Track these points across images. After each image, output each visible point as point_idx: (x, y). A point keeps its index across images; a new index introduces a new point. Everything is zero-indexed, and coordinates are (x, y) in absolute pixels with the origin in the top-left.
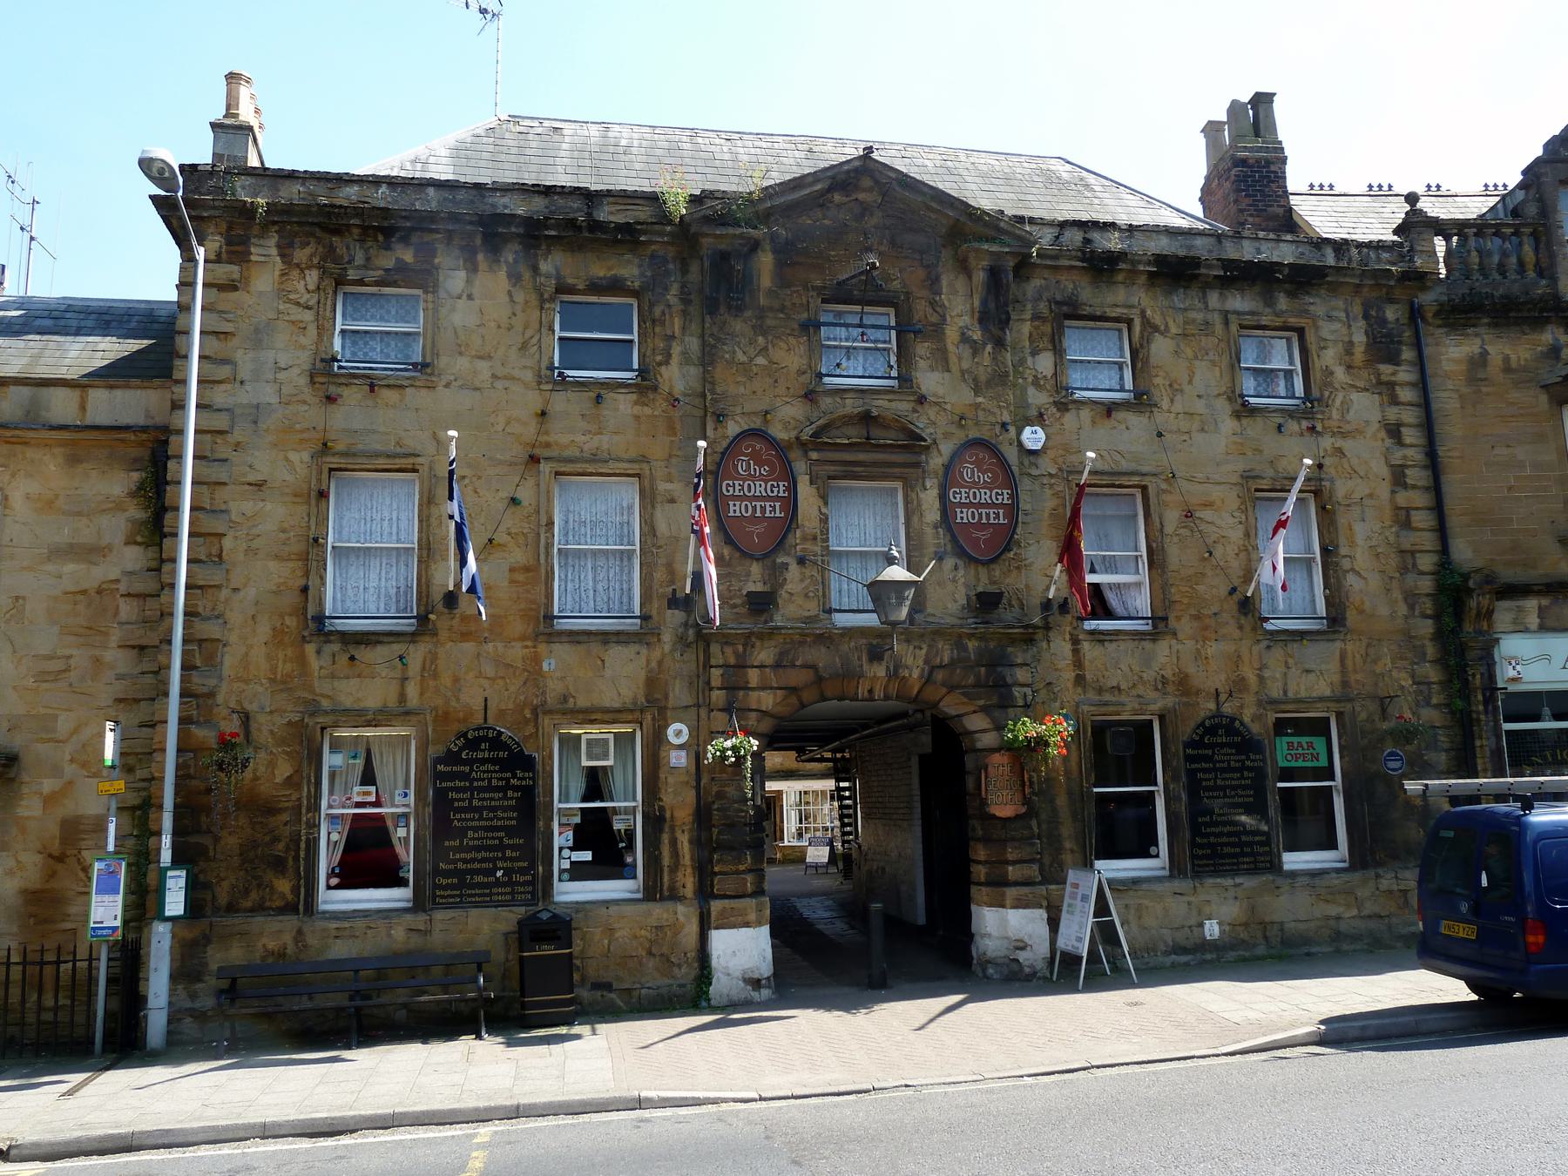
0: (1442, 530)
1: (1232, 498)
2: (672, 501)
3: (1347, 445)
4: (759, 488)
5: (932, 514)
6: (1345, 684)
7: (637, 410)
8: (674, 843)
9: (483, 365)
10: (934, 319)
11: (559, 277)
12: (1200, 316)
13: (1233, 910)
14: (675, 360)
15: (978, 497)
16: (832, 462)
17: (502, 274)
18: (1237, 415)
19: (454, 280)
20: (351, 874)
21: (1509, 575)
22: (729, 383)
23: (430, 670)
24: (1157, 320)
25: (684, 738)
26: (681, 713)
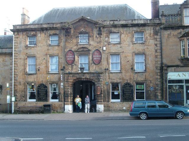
0: (162, 58)
1: (131, 55)
2: (62, 58)
3: (149, 47)
4: (71, 57)
5: (91, 59)
6: (145, 79)
7: (58, 48)
8: (61, 96)
9: (42, 44)
10: (92, 35)
11: (50, 34)
12: (129, 31)
13: (128, 106)
14: (62, 42)
15: (97, 57)
16: (79, 53)
17: (44, 34)
18: (133, 44)
19: (39, 35)
20: (30, 98)
21: (170, 64)
22: (68, 45)
23: (37, 77)
24: (122, 32)
25: (63, 85)
26: (62, 82)
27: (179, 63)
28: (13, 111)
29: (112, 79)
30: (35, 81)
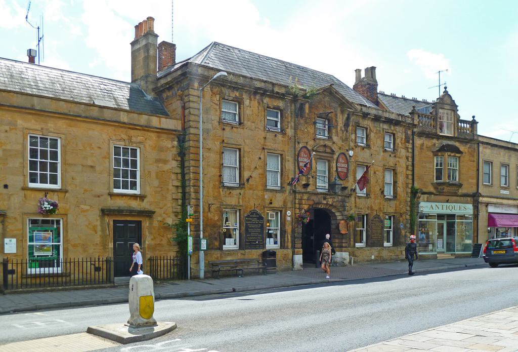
8: (288, 237)
9: (253, 124)
18: (384, 152)
27: (432, 189)
28: (202, 275)
29: (358, 209)
30: (241, 204)
